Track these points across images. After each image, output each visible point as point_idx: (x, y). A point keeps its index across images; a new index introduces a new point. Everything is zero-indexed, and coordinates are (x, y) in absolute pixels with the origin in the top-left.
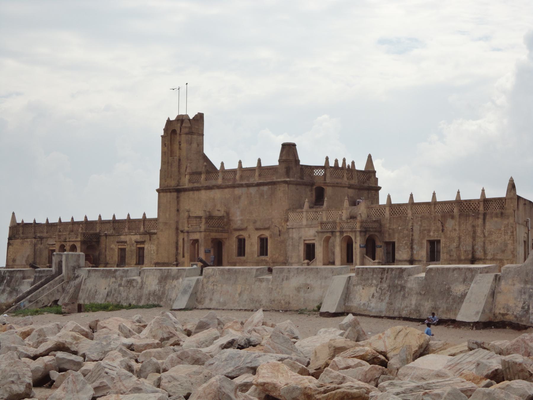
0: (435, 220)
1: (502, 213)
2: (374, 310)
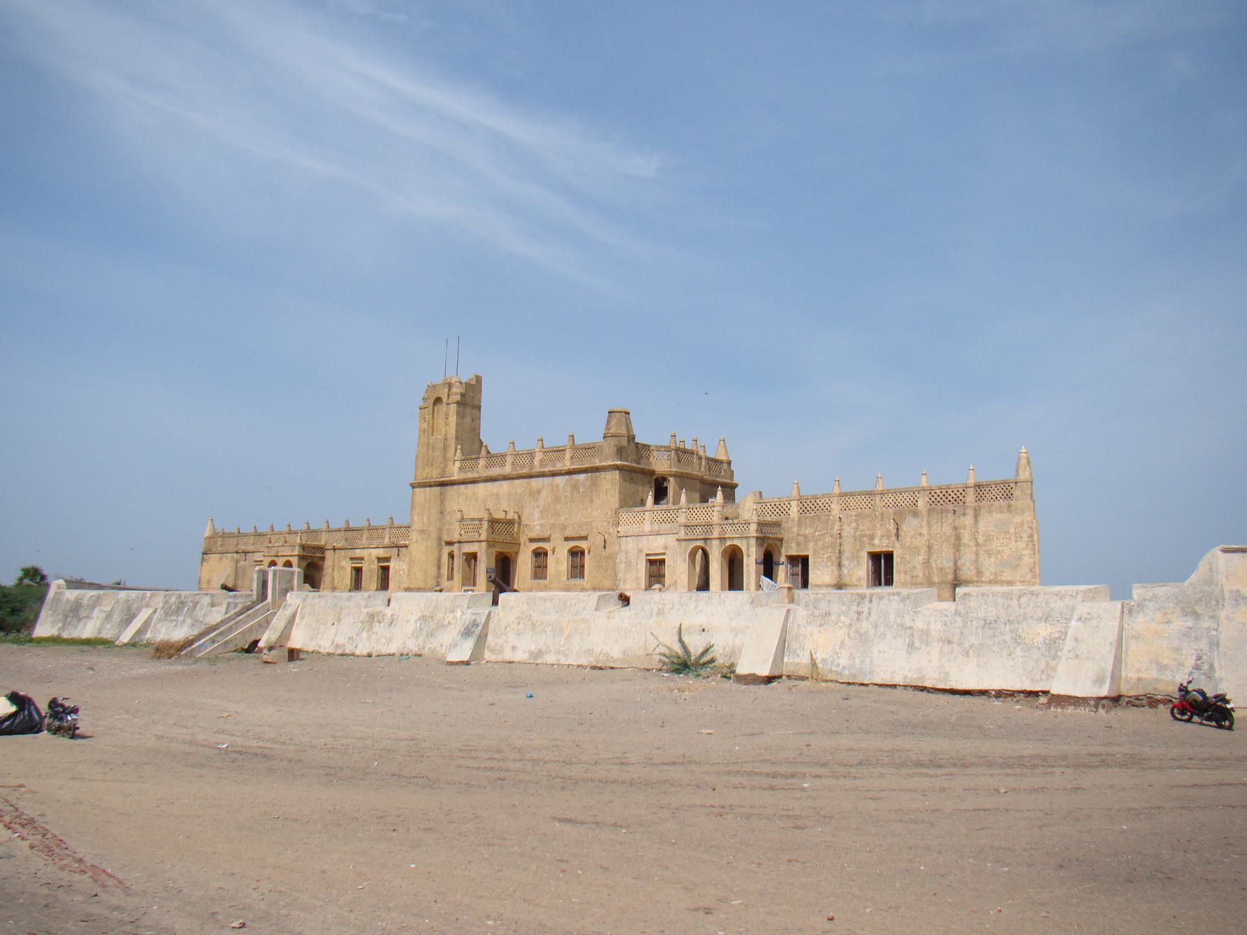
0: (882, 519)
1: (1009, 506)
2: (846, 672)
